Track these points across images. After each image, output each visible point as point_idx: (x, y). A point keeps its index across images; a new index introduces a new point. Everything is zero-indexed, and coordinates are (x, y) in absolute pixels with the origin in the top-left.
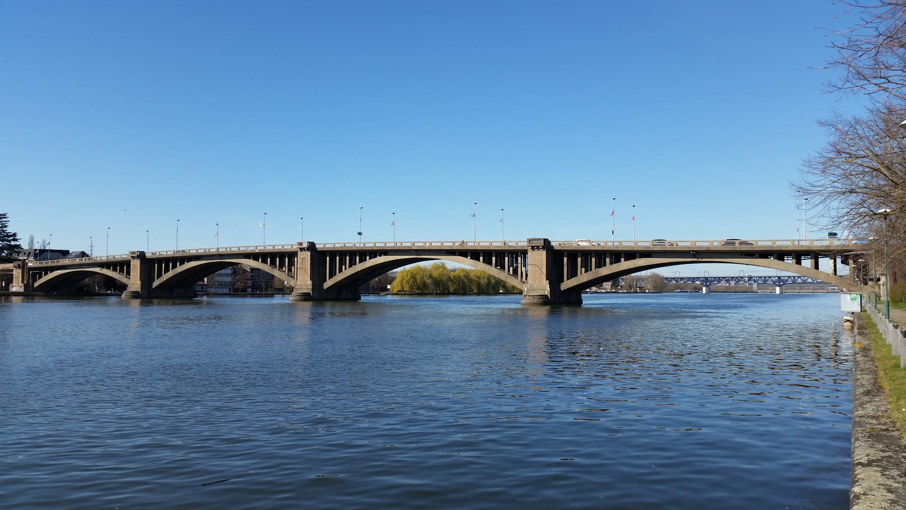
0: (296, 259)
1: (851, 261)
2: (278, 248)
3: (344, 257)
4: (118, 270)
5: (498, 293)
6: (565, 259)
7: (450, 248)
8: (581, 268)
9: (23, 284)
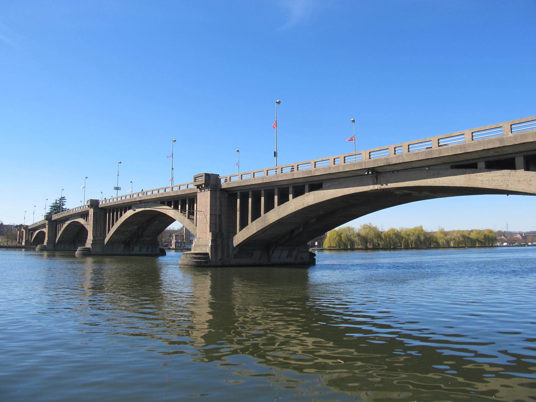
0: (195, 205)
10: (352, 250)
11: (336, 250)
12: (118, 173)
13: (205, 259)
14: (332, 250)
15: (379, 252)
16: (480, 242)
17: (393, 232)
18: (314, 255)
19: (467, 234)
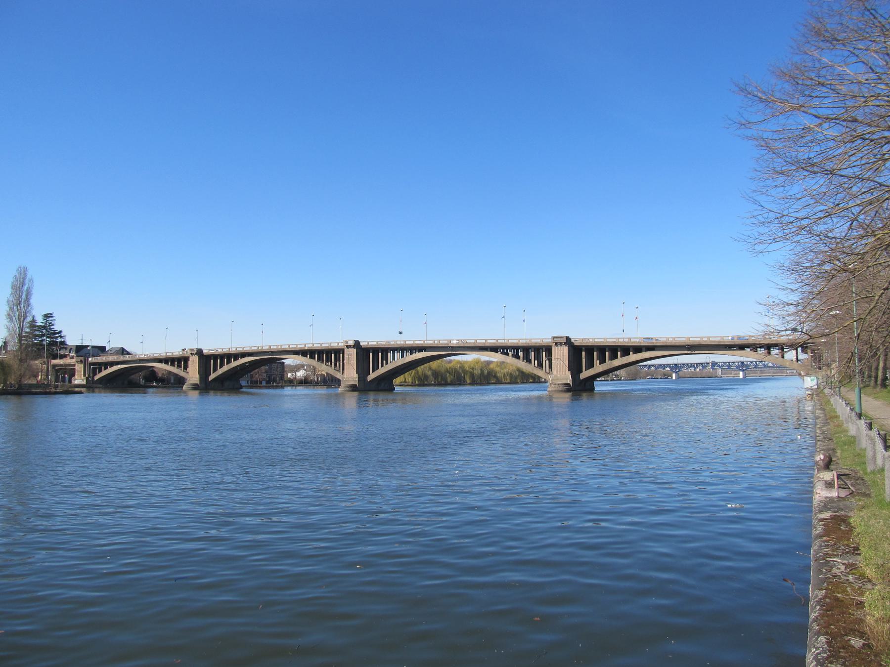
1: (809, 351)
2: (325, 346)
3: (321, 355)
4: (176, 365)
5: (489, 384)
6: (584, 353)
7: (483, 345)
8: (597, 360)
9: (85, 378)
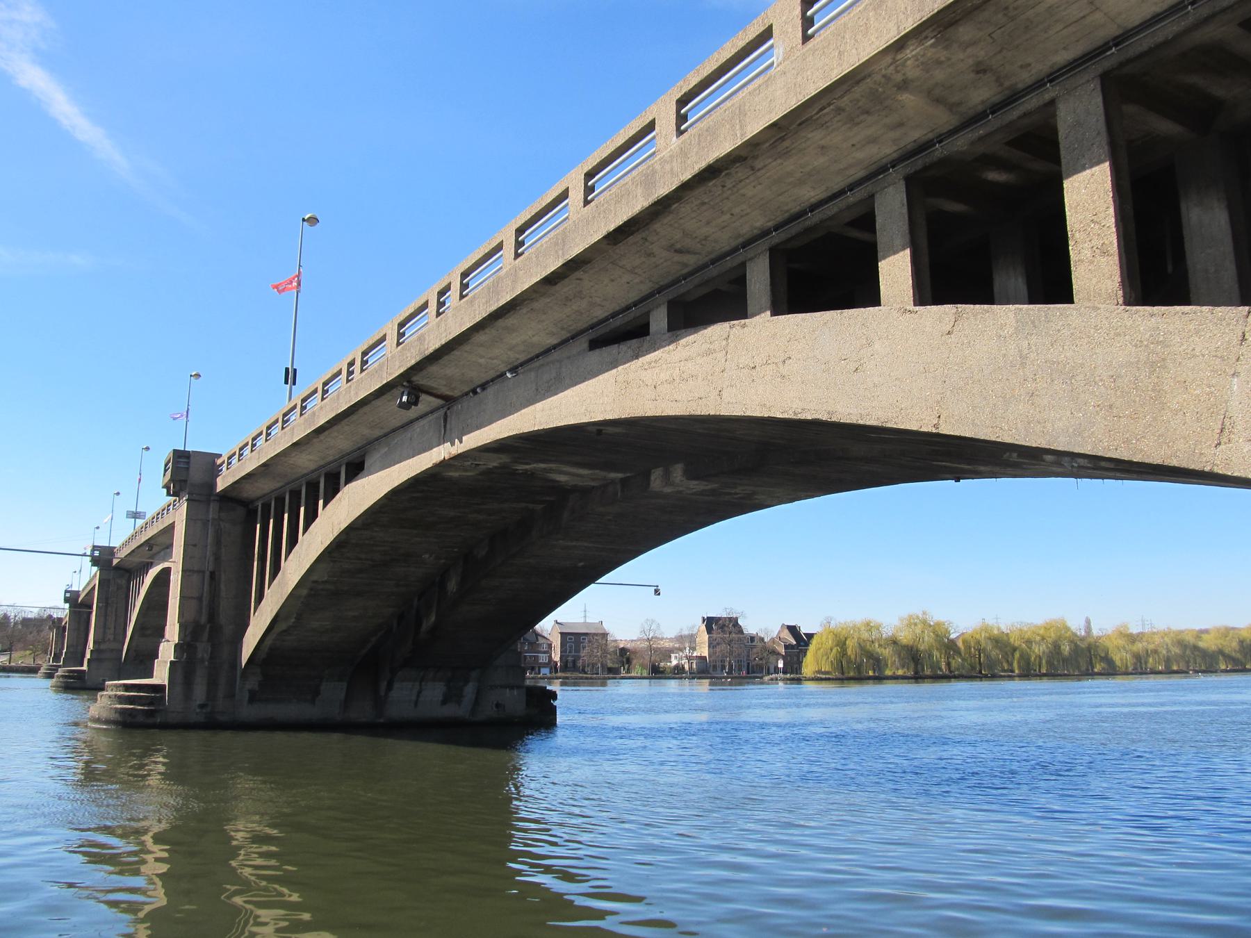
10: (1052, 678)
11: (833, 679)
12: (140, 474)
13: (149, 705)
14: (821, 679)
15: (982, 683)
16: (1228, 658)
17: (987, 635)
18: (553, 695)
19: (1190, 639)
